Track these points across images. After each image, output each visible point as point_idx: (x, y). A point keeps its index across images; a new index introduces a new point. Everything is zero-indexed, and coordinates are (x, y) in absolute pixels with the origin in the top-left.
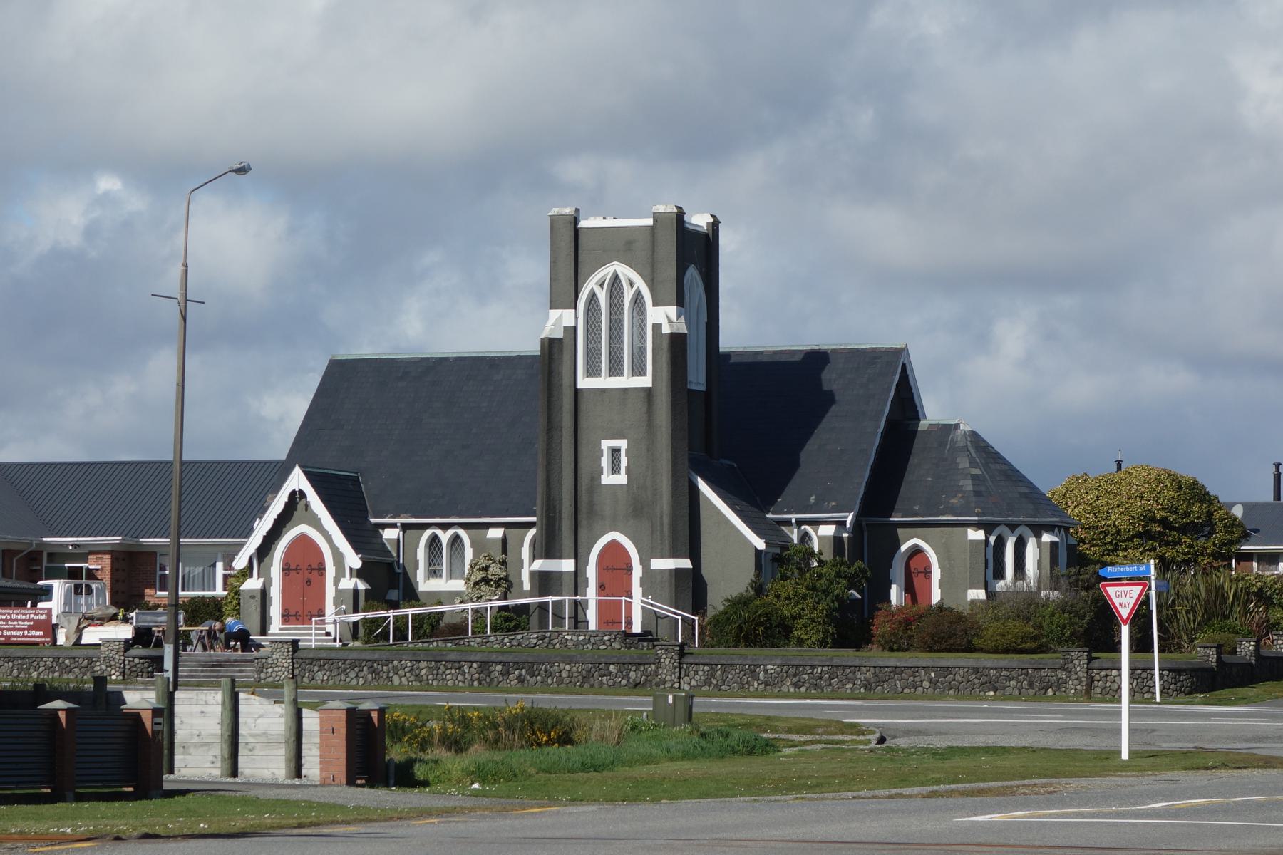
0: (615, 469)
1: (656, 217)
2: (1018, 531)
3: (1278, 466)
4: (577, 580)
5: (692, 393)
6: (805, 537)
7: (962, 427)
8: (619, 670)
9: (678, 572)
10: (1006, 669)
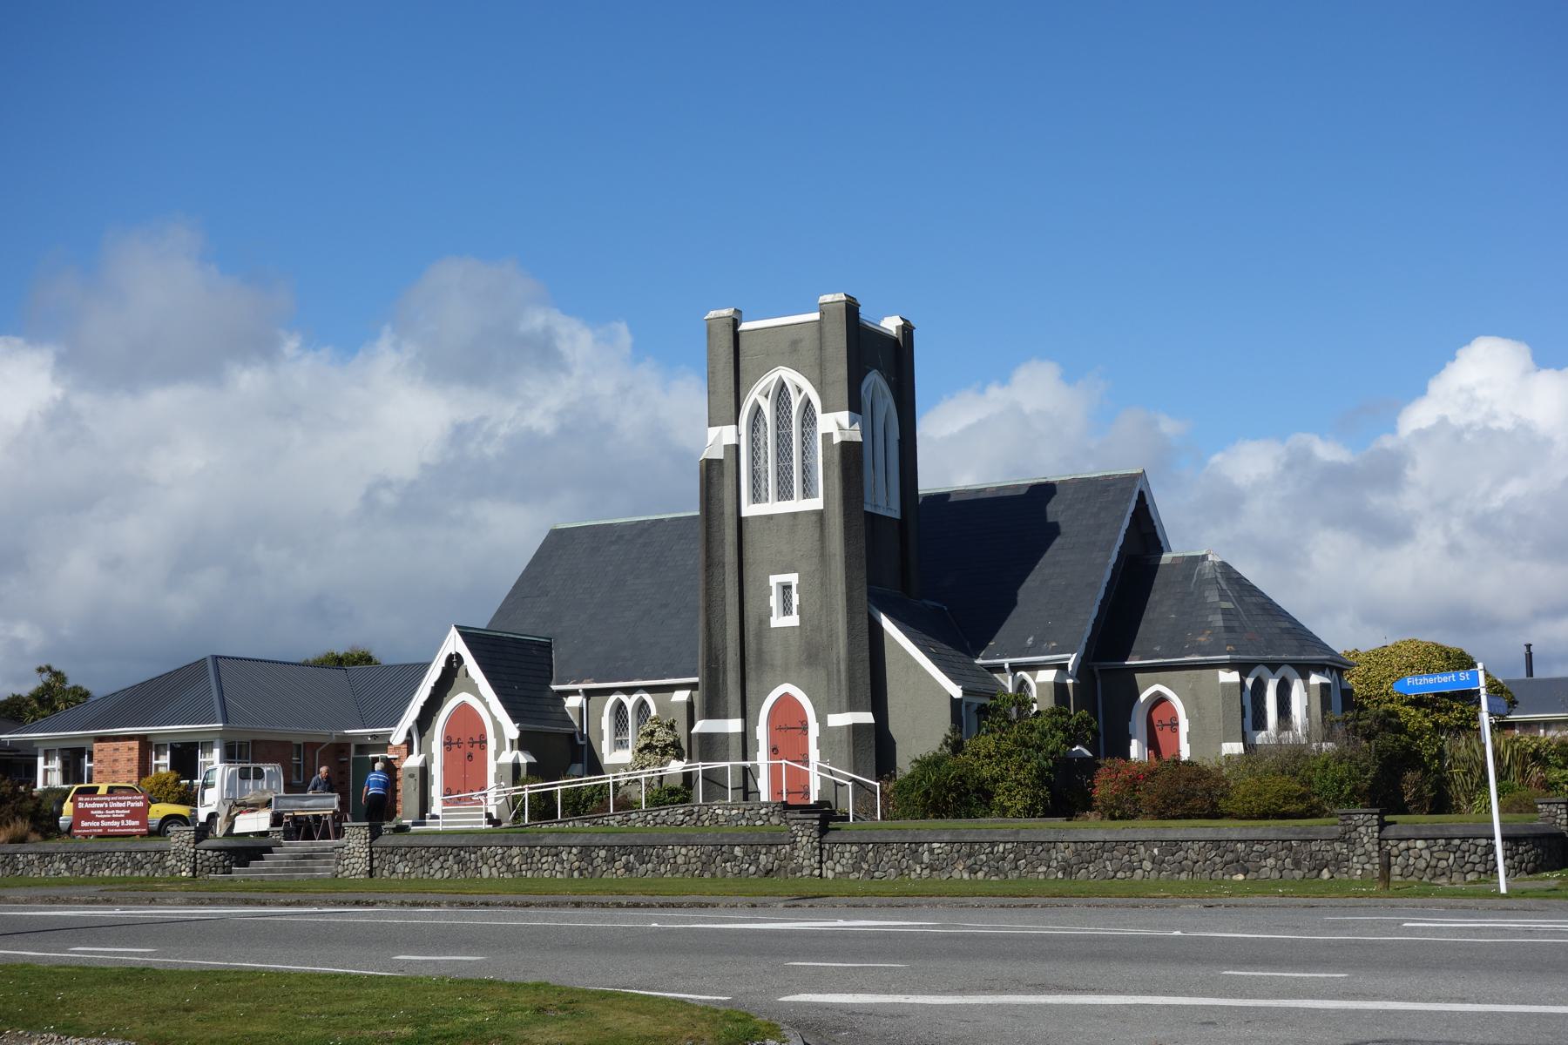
0: (787, 610)
1: (823, 310)
2: (1282, 671)
3: (1528, 646)
4: (746, 742)
5: (872, 518)
6: (1022, 686)
7: (1210, 558)
8: (746, 853)
9: (856, 728)
10: (1260, 841)
